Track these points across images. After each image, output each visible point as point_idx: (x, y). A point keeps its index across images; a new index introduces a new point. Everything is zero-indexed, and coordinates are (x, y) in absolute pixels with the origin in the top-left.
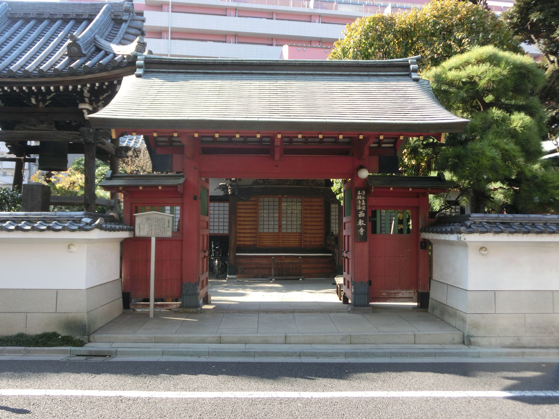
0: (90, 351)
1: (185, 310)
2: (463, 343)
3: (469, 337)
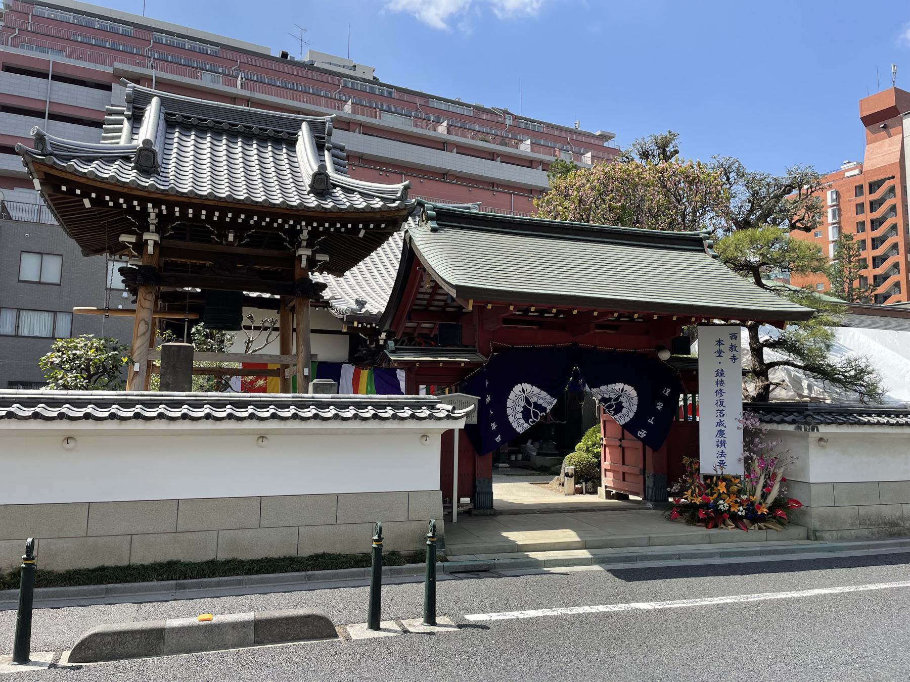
1: (482, 511)
2: (808, 538)
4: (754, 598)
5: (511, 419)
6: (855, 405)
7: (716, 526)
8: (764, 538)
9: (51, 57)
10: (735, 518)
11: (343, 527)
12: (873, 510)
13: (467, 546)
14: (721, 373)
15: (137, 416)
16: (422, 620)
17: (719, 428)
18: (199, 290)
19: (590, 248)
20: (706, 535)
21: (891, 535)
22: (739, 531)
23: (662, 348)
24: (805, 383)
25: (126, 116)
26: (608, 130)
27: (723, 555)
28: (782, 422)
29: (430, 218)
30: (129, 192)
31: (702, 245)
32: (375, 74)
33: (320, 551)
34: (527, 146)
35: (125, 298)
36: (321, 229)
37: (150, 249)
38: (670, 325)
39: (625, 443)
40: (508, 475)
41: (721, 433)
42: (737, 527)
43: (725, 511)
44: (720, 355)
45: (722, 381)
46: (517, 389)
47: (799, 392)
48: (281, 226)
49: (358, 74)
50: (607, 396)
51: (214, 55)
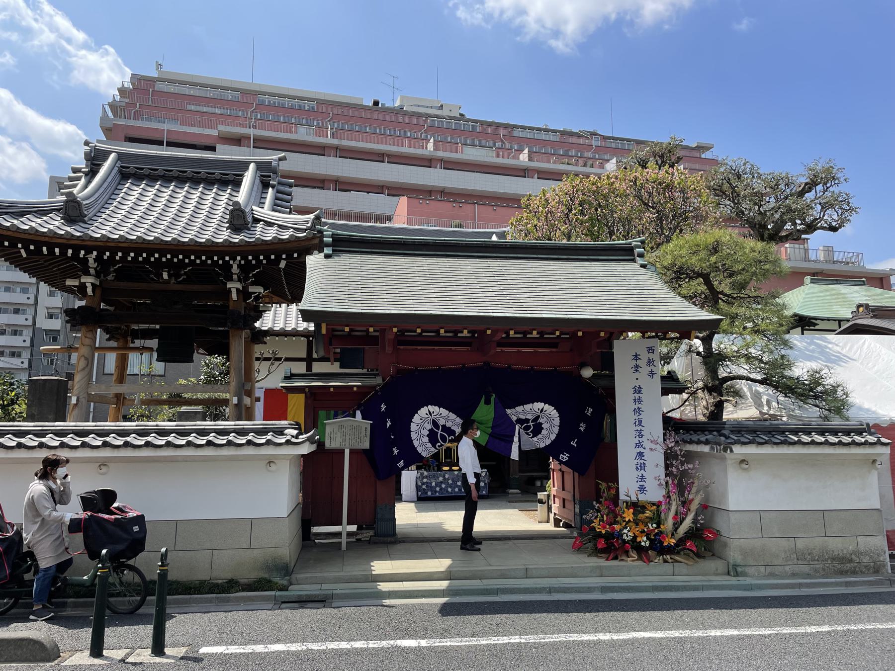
0: (300, 596)
1: (382, 539)
2: (729, 574)
3: (735, 566)
4: (549, 639)
5: (416, 443)
6: (821, 419)
7: (616, 558)
8: (671, 572)
9: (166, 126)
10: (639, 549)
11: (180, 554)
12: (816, 543)
13: (325, 575)
14: (638, 390)
16: (149, 651)
17: (638, 450)
18: (158, 327)
19: (495, 265)
20: (597, 567)
21: (842, 573)
22: (641, 563)
23: (583, 365)
24: (764, 399)
25: (83, 172)
26: (704, 141)
27: (604, 589)
28: (699, 442)
30: (66, 242)
31: (633, 255)
36: (187, 261)
38: (594, 341)
40: (509, 502)
41: (641, 455)
43: (628, 542)
44: (636, 371)
45: (640, 398)
46: (423, 411)
48: (146, 260)
49: (445, 112)
50: (523, 417)
51: (311, 110)
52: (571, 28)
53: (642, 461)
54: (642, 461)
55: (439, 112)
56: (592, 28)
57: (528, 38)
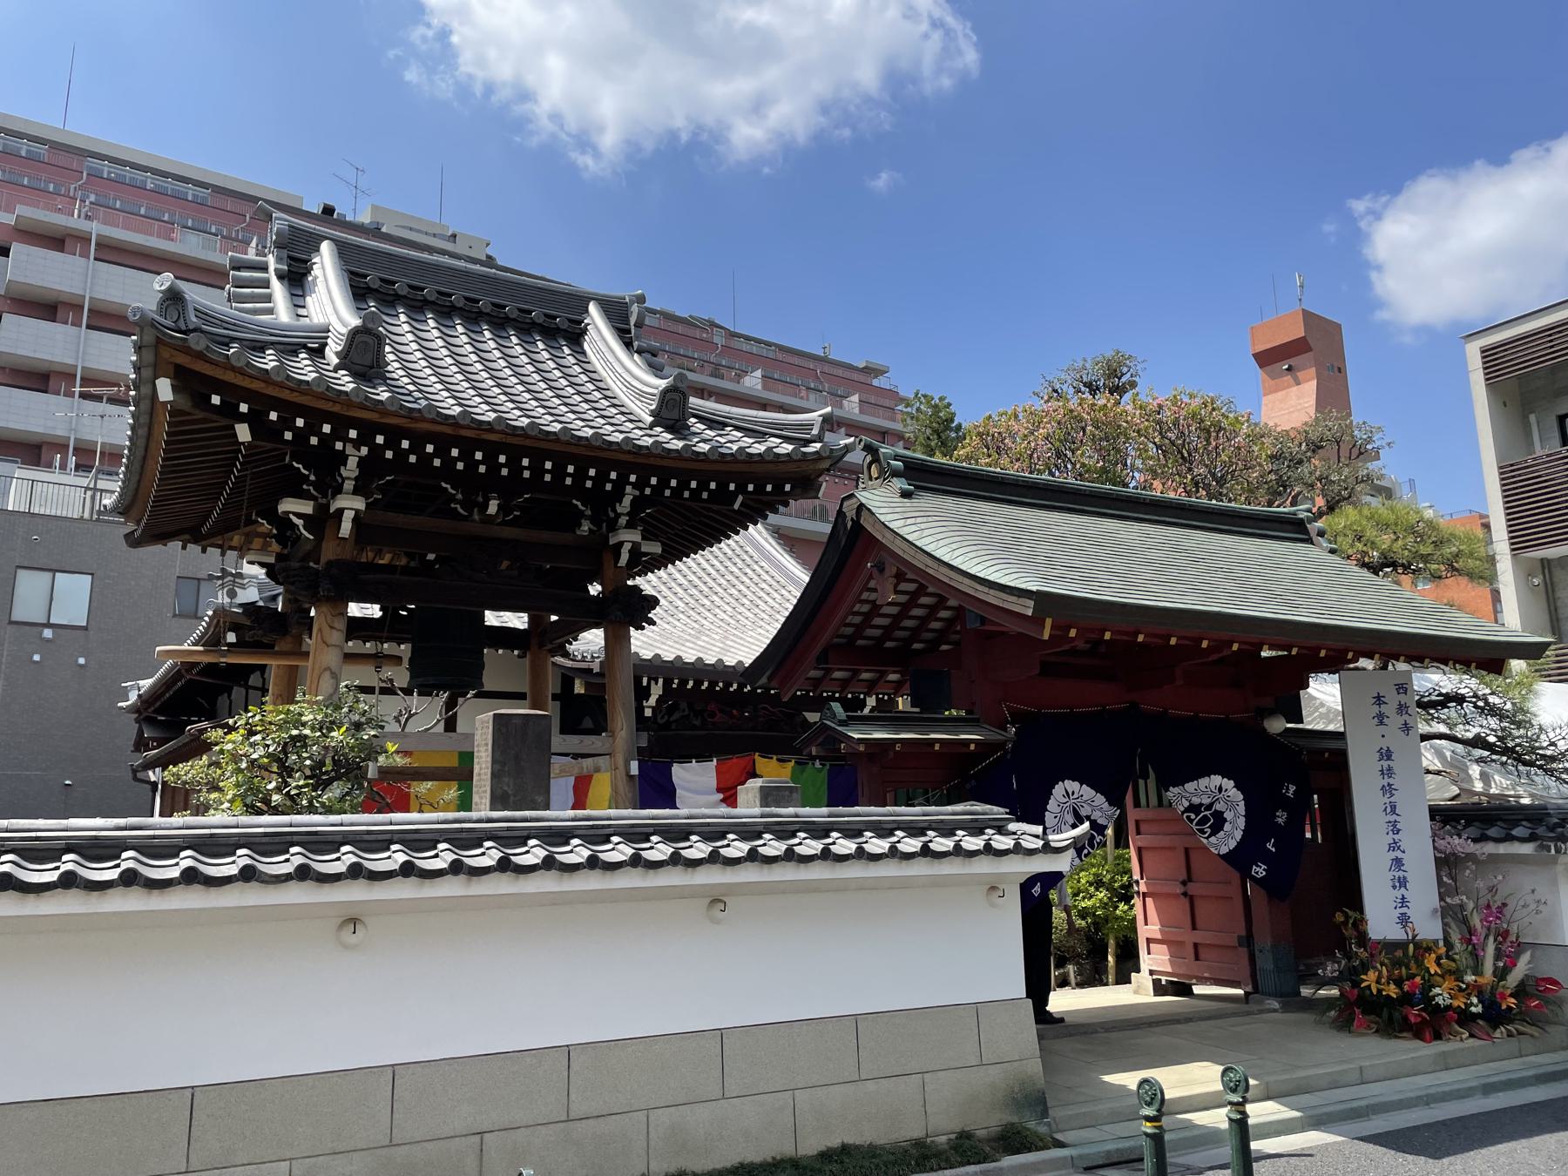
10: (1465, 1018)
14: (1387, 755)
15: (130, 879)
17: (1393, 855)
24: (1475, 770)
26: (878, 361)
28: (1509, 838)
29: (896, 474)
31: (1306, 532)
32: (489, 251)
33: (835, 1142)
34: (755, 381)
35: (48, 640)
37: (346, 528)
39: (1193, 888)
41: (1398, 862)
42: (1472, 1036)
44: (1381, 723)
45: (1390, 769)
47: (1465, 786)
50: (1196, 801)
52: (609, 140)
53: (1401, 874)
54: (1401, 874)
55: (449, 246)
56: (649, 145)
57: (534, 142)
